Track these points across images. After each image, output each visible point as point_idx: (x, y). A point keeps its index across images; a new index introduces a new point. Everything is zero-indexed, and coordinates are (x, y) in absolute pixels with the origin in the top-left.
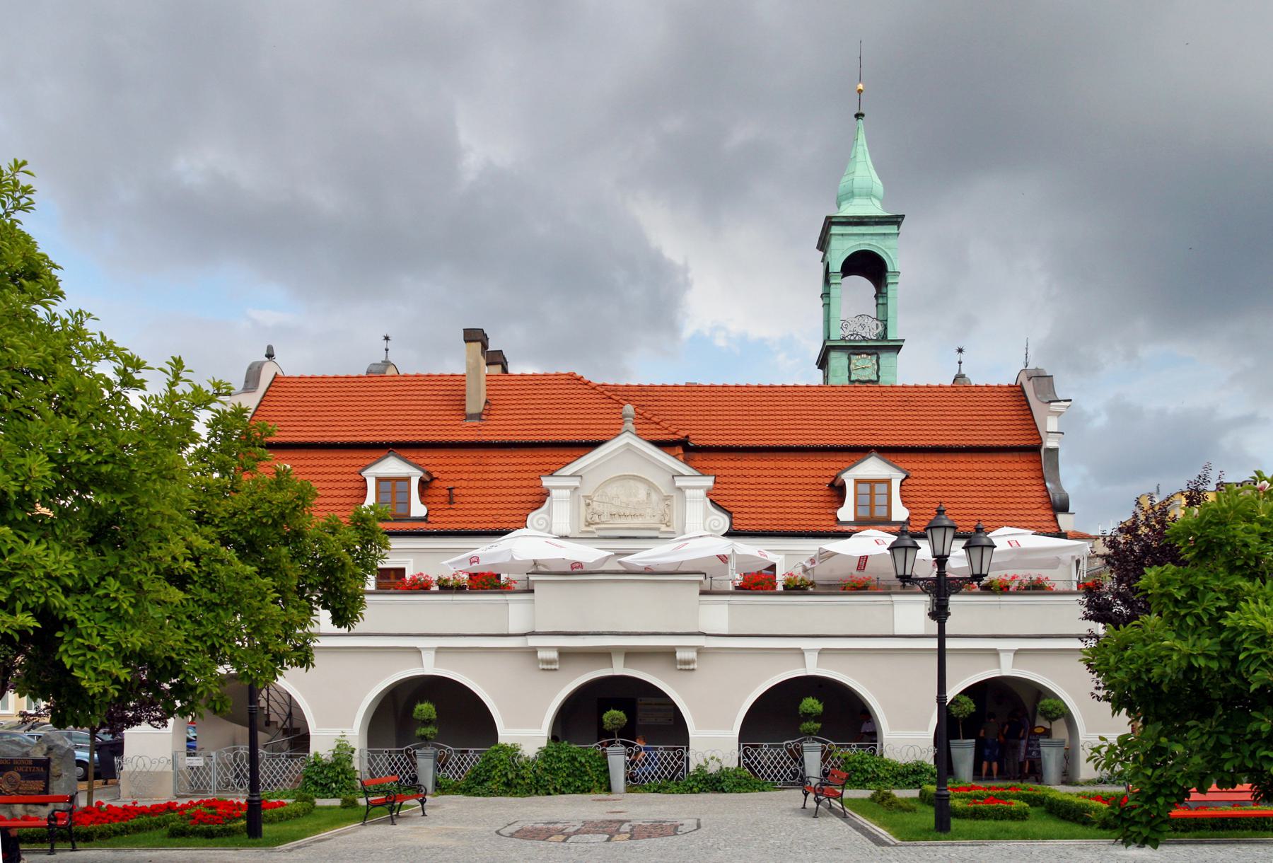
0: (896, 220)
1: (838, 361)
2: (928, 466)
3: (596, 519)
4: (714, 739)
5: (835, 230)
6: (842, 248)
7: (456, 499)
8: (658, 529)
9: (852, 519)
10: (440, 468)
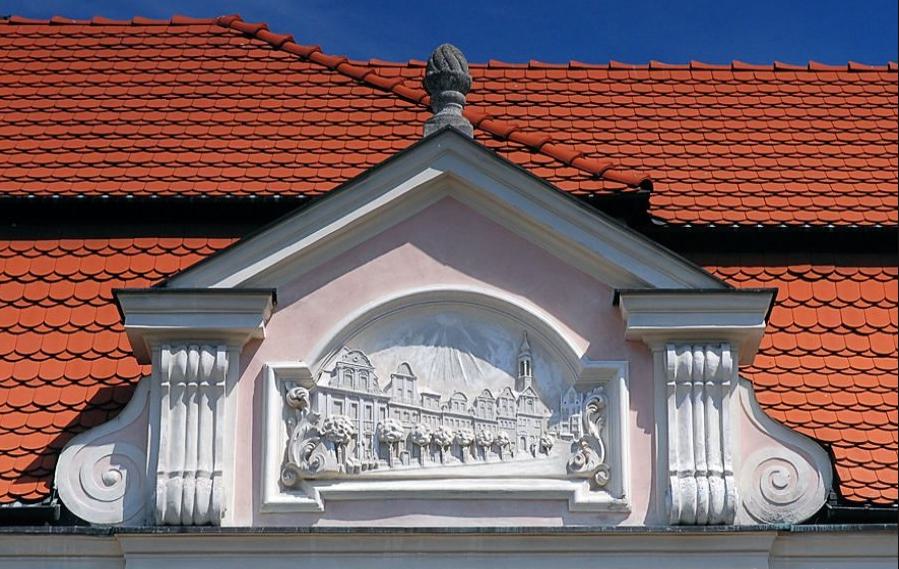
3: (328, 460)
8: (560, 501)
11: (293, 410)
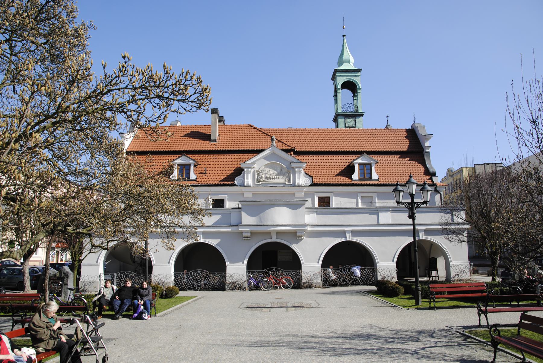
0: (359, 71)
1: (341, 121)
2: (384, 158)
4: (311, 266)
5: (337, 74)
6: (341, 80)
7: (207, 172)
9: (358, 179)
10: (201, 160)
11: (258, 174)
